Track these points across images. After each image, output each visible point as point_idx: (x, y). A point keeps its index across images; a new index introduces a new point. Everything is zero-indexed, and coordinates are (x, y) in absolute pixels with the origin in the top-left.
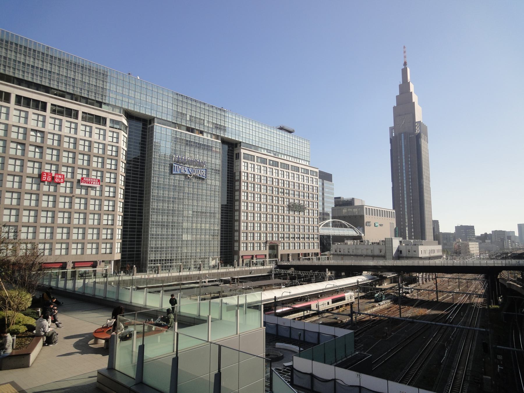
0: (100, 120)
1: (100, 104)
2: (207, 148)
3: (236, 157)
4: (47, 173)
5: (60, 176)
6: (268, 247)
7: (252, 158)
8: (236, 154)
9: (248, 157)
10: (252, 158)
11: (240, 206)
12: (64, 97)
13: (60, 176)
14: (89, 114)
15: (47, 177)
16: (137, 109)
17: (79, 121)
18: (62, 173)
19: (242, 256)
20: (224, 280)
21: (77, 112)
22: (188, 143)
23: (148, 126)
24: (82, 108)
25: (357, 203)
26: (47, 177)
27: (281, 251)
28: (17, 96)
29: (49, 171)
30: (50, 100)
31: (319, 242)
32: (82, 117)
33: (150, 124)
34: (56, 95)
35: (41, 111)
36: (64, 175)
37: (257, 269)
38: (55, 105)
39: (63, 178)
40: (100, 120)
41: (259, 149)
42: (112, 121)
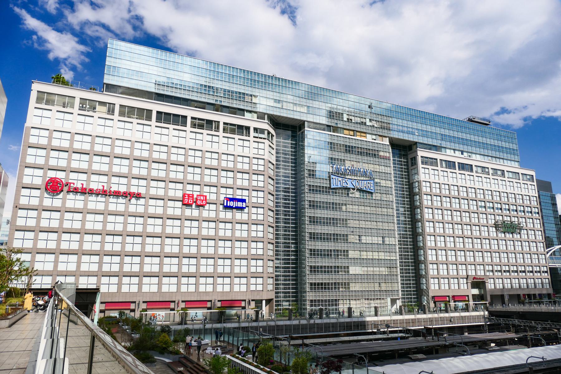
0: (243, 130)
1: (241, 111)
2: (371, 153)
3: (412, 163)
4: (189, 195)
5: (202, 198)
6: (470, 285)
7: (432, 162)
8: (412, 159)
9: (427, 161)
10: (432, 162)
11: (423, 227)
12: (204, 109)
13: (202, 198)
14: (231, 124)
15: (188, 199)
16: (284, 114)
17: (188, 128)
18: (205, 194)
19: (433, 297)
20: (414, 330)
21: (185, 117)
22: (349, 149)
23: (298, 133)
24: (222, 118)
25: (278, 9)
26: (188, 199)
27: (490, 286)
28: (158, 112)
29: (191, 193)
30: (190, 113)
31: (549, 277)
32: (224, 129)
33: (300, 130)
34: (196, 107)
35: (146, 120)
36: (206, 196)
37: (457, 317)
38: (195, 118)
39: (206, 200)
40: (243, 130)
41: (443, 150)
42: (256, 130)
